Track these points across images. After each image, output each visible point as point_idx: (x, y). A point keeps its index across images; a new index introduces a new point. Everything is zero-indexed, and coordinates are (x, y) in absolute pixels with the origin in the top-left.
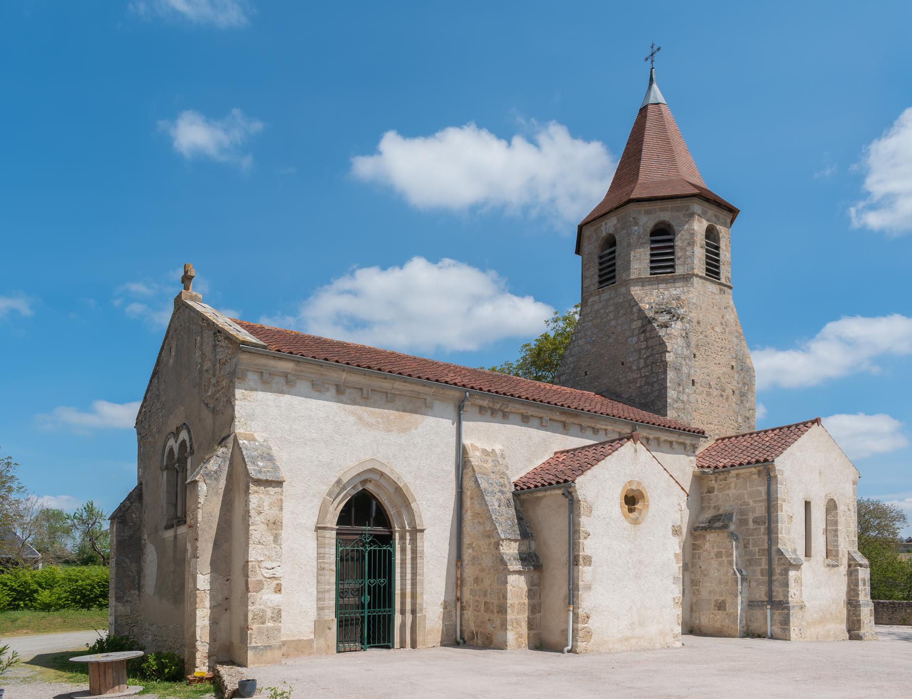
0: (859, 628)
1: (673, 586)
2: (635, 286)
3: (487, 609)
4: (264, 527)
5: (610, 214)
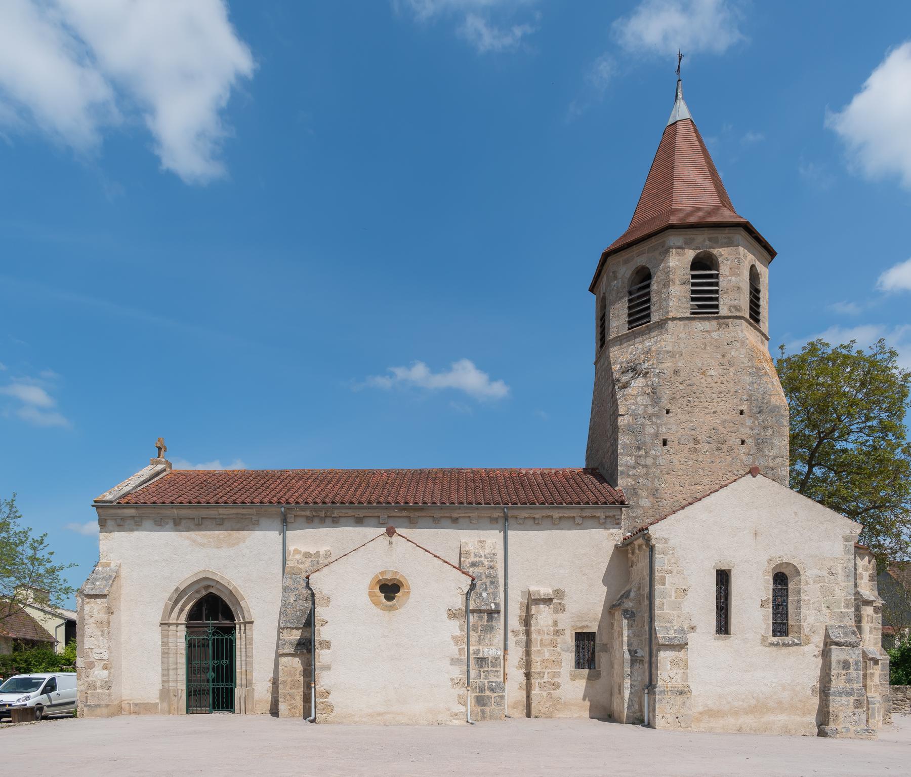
4: (94, 625)
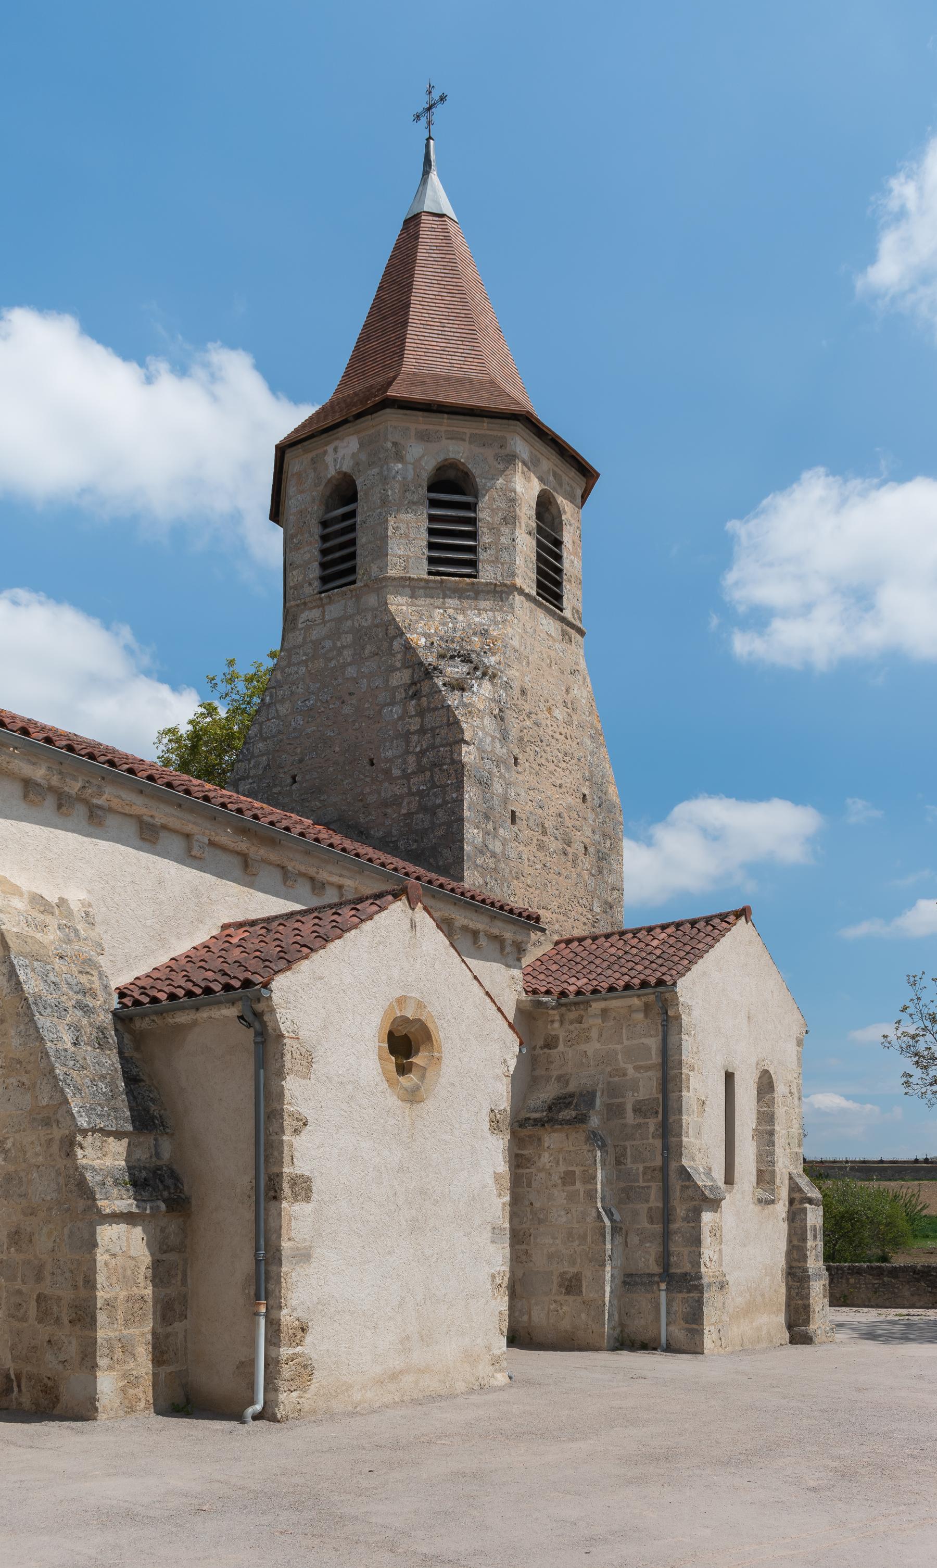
0: (807, 1322)
1: (492, 1248)
2: (397, 593)
3: (44, 1315)
5: (344, 427)
